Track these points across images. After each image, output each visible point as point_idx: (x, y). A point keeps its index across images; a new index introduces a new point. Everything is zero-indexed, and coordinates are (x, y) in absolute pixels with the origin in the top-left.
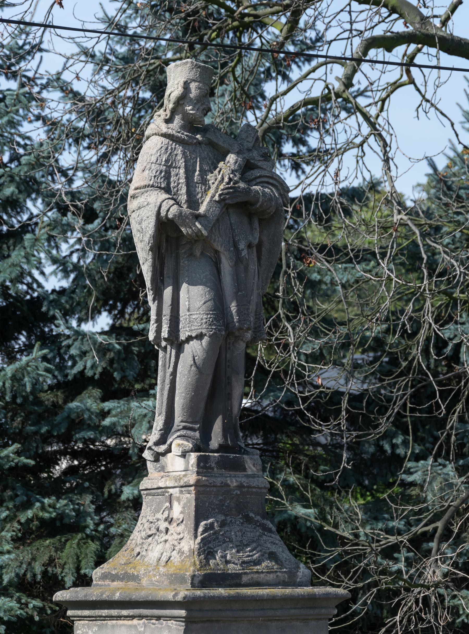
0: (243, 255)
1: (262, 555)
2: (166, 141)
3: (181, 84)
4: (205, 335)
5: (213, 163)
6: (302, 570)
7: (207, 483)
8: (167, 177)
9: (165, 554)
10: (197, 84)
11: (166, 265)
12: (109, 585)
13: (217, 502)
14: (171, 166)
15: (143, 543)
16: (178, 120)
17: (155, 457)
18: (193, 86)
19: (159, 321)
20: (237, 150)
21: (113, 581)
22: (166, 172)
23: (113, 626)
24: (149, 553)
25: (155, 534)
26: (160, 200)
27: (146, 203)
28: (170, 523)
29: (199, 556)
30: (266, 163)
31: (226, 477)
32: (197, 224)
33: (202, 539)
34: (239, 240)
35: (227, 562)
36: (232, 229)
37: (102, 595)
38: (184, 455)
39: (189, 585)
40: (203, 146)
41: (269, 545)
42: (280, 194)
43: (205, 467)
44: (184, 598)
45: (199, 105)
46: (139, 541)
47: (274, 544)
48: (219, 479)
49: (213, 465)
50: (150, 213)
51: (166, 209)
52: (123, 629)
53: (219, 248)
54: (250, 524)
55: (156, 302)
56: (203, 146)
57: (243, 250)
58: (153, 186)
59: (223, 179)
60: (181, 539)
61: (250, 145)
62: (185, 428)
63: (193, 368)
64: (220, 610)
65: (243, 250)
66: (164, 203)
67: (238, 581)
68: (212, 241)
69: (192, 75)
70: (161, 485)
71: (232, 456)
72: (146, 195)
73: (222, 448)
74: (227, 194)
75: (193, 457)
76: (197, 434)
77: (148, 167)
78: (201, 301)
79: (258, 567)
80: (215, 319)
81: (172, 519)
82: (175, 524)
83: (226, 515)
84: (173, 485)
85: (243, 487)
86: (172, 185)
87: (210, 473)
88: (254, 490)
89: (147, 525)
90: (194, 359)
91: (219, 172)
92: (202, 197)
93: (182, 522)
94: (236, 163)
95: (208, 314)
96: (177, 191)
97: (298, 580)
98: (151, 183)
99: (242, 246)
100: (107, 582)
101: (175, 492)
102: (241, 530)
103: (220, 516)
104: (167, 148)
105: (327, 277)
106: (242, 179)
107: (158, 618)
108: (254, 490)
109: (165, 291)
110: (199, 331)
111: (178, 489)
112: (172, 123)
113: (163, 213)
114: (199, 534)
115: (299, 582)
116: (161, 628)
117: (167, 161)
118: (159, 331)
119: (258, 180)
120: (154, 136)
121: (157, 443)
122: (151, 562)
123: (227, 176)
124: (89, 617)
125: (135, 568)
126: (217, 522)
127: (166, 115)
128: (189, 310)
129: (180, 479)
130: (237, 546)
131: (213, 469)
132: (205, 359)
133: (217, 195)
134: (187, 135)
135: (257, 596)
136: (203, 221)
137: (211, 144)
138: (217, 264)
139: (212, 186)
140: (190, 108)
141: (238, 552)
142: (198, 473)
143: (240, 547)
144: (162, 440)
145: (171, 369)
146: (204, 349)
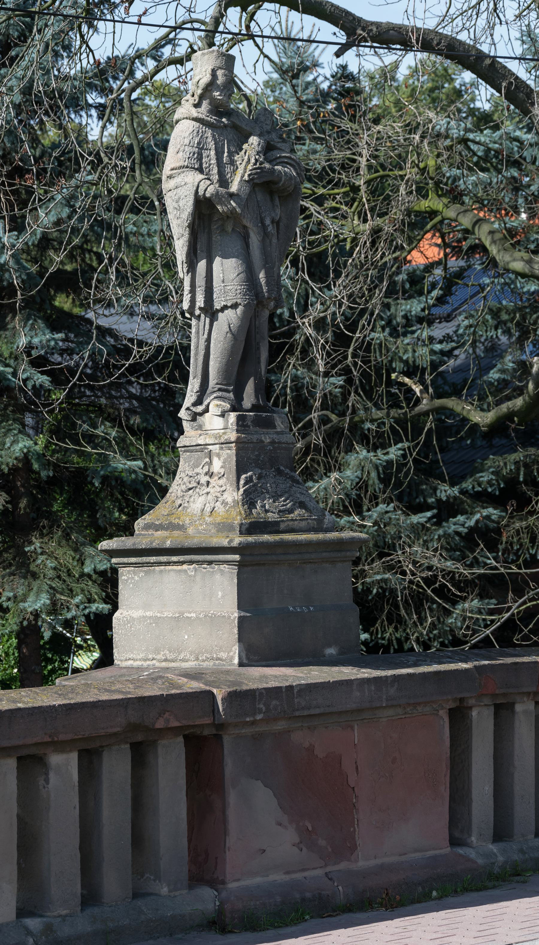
0: (269, 230)
1: (294, 505)
2: (197, 124)
3: (209, 71)
4: (240, 304)
5: (238, 145)
6: (327, 517)
7: (245, 440)
8: (200, 158)
9: (208, 505)
10: (223, 71)
11: (199, 240)
12: (153, 534)
13: (254, 457)
14: (202, 148)
15: (183, 495)
16: (205, 105)
17: (192, 417)
18: (220, 73)
19: (193, 291)
20: (259, 132)
21: (157, 531)
22: (198, 153)
23: (161, 571)
24: (191, 504)
25: (196, 487)
26: (197, 181)
27: (183, 183)
28: (211, 476)
29: (243, 506)
30: (284, 144)
31: (261, 434)
32: (232, 202)
33: (245, 491)
34: (265, 216)
35: (267, 511)
36: (259, 206)
37: (152, 543)
38: (223, 415)
39: (238, 532)
40: (229, 129)
41: (298, 495)
42: (297, 173)
43: (243, 426)
44: (240, 544)
45: (226, 91)
46: (180, 493)
47: (302, 494)
48: (255, 436)
49: (250, 423)
50: (188, 193)
51: (204, 188)
52: (172, 574)
53: (248, 224)
54: (281, 476)
55: (190, 274)
56: (229, 129)
57: (269, 226)
58: (187, 167)
59: (249, 161)
60: (223, 491)
61: (269, 127)
62: (220, 390)
63: (229, 335)
64: (267, 554)
65: (269, 226)
66: (202, 183)
67: (277, 528)
68: (242, 218)
69: (218, 63)
70: (200, 442)
71: (264, 414)
72: (182, 175)
73: (255, 408)
74: (255, 174)
75: (232, 417)
76: (231, 395)
77: (182, 149)
78: (234, 273)
79: (292, 515)
80: (248, 289)
81: (212, 473)
82: (216, 478)
83: (262, 469)
84: (213, 443)
85: (275, 443)
86: (204, 166)
87: (247, 430)
88: (284, 445)
89: (186, 479)
90: (230, 327)
91: (245, 153)
92: (231, 177)
93: (223, 475)
94: (259, 144)
95: (241, 285)
96: (209, 171)
97: (325, 526)
98: (186, 164)
99: (268, 222)
100: (151, 532)
101: (215, 449)
102: (275, 482)
103: (257, 469)
104: (198, 132)
105: (143, 229)
106: (266, 159)
107: (210, 563)
108: (284, 445)
109: (199, 264)
110: (235, 301)
111: (218, 446)
112: (200, 107)
113: (201, 193)
114: (241, 486)
115: (326, 528)
116: (213, 572)
117: (199, 143)
118: (193, 301)
119: (278, 161)
120: (185, 120)
121: (195, 404)
122: (195, 513)
123: (254, 158)
124: (136, 564)
125: (179, 518)
126: (255, 475)
127: (195, 100)
128: (223, 282)
129: (221, 436)
130: (273, 497)
131: (249, 427)
132: (239, 326)
133: (246, 175)
134: (215, 119)
135: (297, 541)
136: (236, 200)
137: (235, 127)
138: (245, 238)
139: (239, 166)
140: (218, 93)
141: (274, 502)
142: (238, 431)
143: (276, 497)
144: (199, 402)
145: (206, 336)
146: (239, 318)
